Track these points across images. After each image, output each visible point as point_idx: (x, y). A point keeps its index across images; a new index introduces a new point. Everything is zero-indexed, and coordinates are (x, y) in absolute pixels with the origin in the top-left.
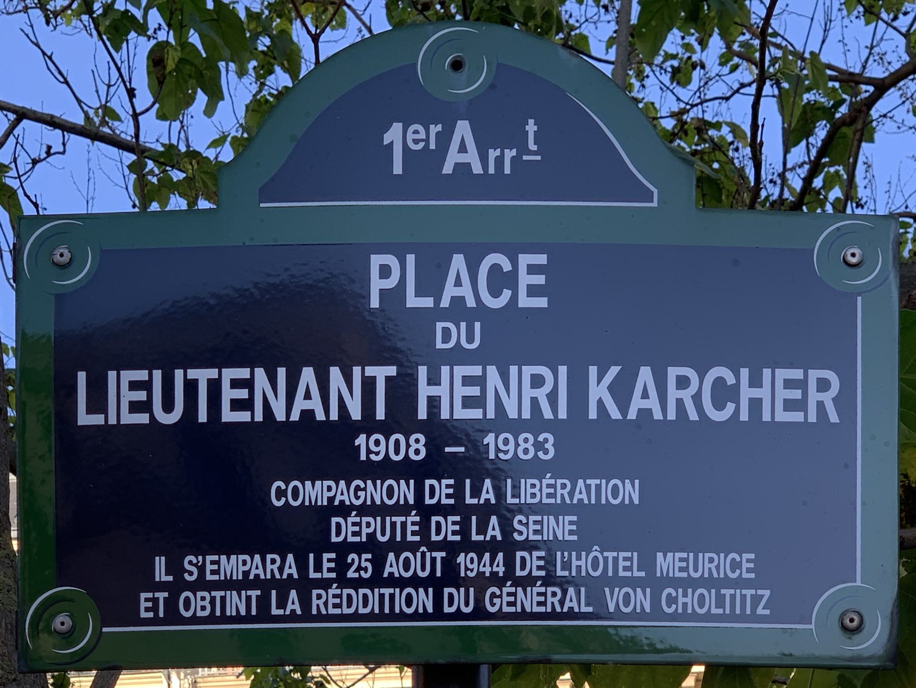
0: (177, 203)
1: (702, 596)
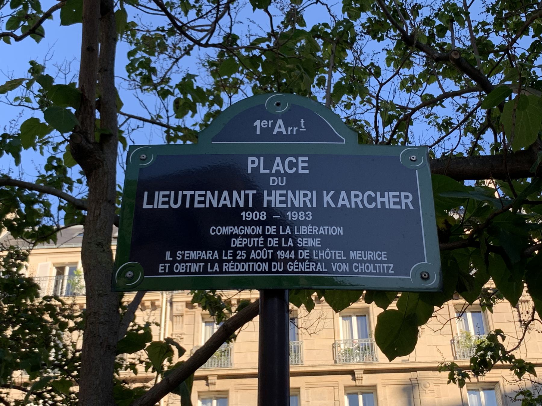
0: (180, 142)
1: (368, 266)
